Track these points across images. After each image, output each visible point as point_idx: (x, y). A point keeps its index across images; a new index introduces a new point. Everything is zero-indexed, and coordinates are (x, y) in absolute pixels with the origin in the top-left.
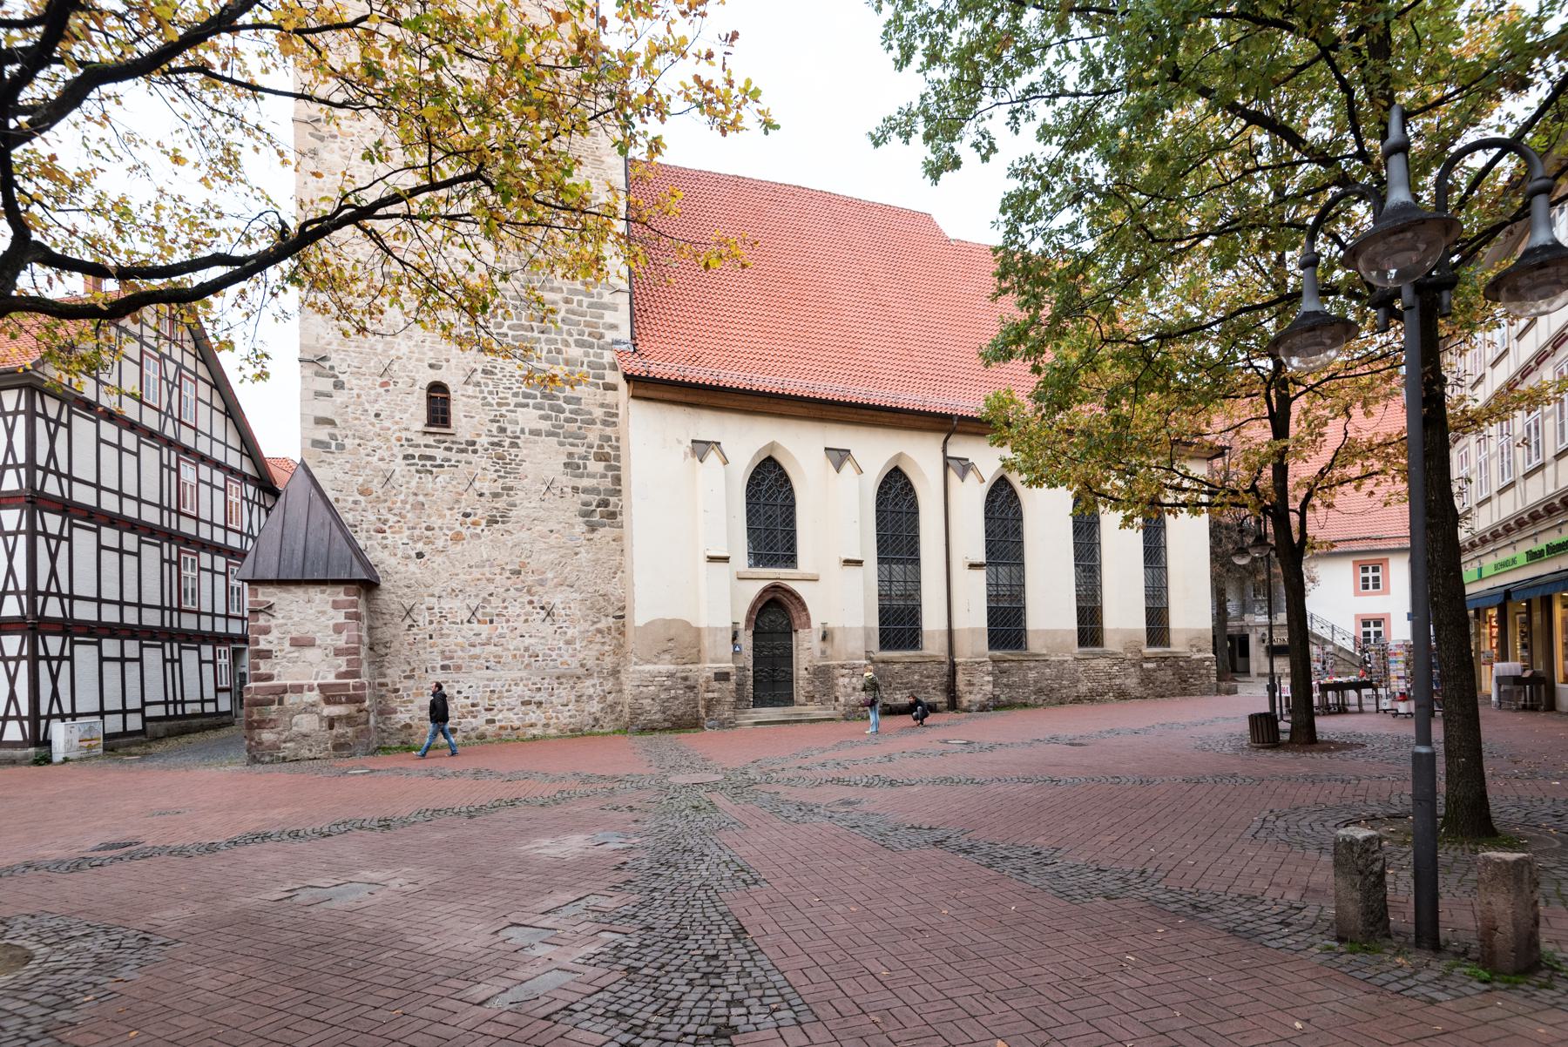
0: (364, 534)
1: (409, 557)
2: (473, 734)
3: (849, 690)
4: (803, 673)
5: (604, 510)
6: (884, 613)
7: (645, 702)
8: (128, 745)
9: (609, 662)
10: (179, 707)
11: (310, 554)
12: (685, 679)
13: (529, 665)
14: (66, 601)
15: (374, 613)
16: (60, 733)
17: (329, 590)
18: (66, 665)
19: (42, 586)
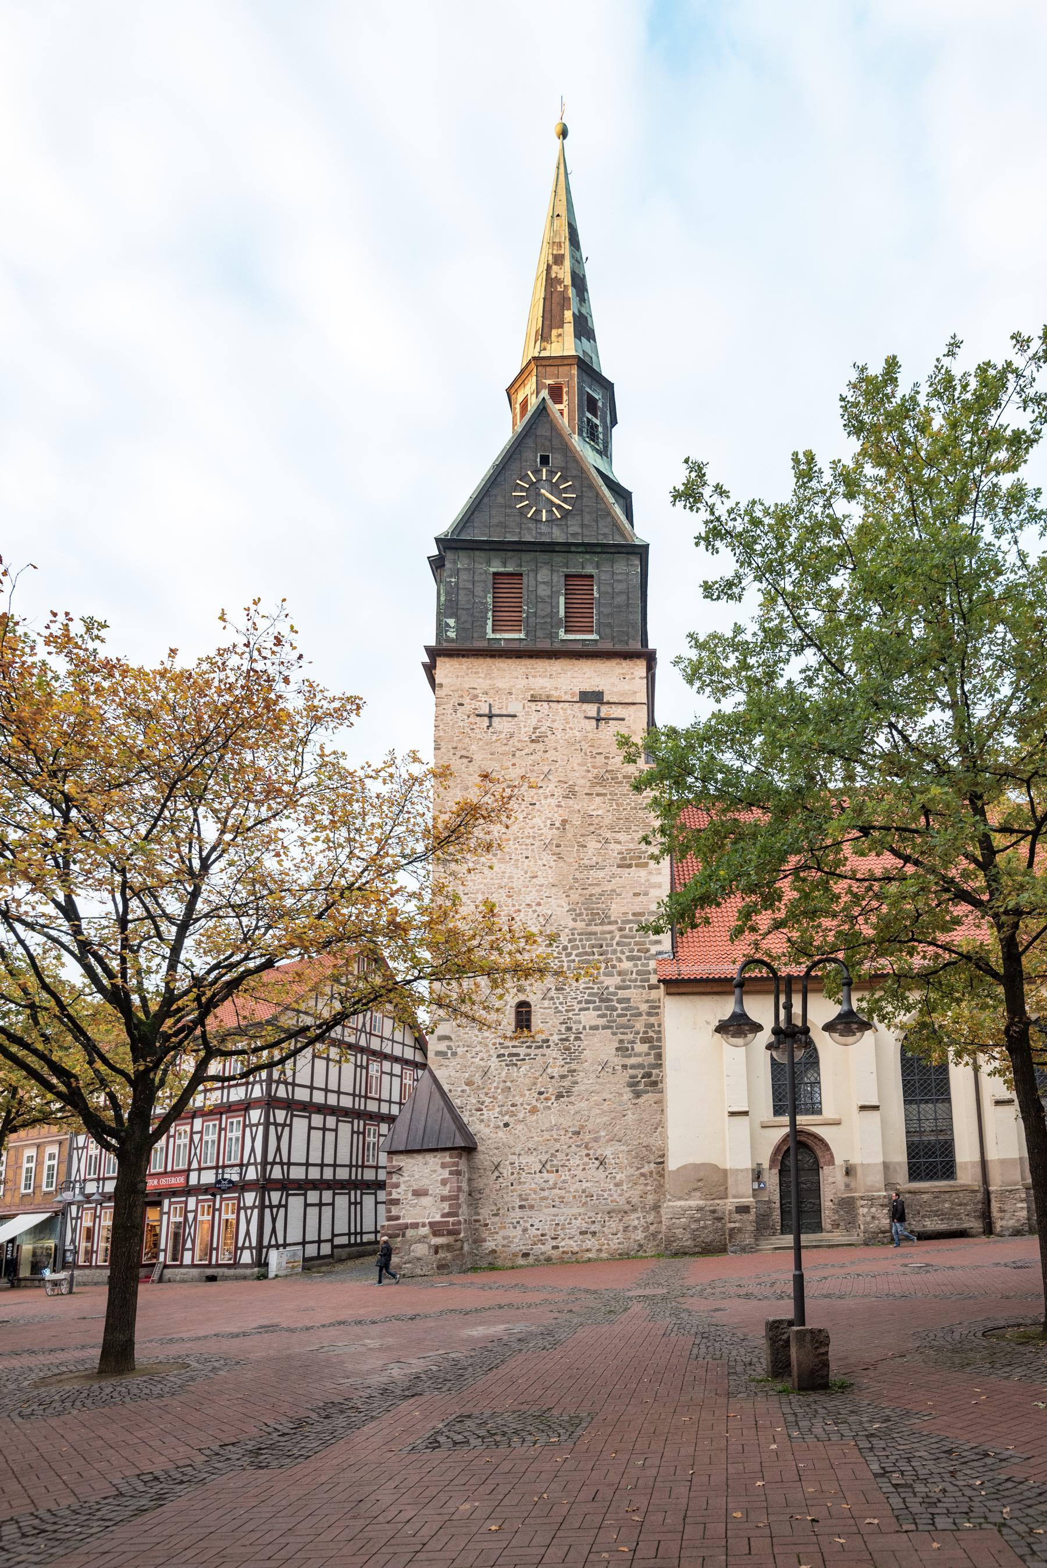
0: (468, 1113)
1: (498, 1127)
2: (542, 1257)
3: (868, 1219)
4: (829, 1204)
5: (648, 1081)
6: (913, 1150)
7: (677, 1231)
8: (320, 1266)
9: (651, 1199)
10: (359, 1237)
11: (427, 1132)
12: (714, 1212)
13: (586, 1203)
14: (285, 1167)
15: (472, 1169)
16: (275, 1259)
17: (439, 1155)
18: (282, 1210)
19: (270, 1159)
